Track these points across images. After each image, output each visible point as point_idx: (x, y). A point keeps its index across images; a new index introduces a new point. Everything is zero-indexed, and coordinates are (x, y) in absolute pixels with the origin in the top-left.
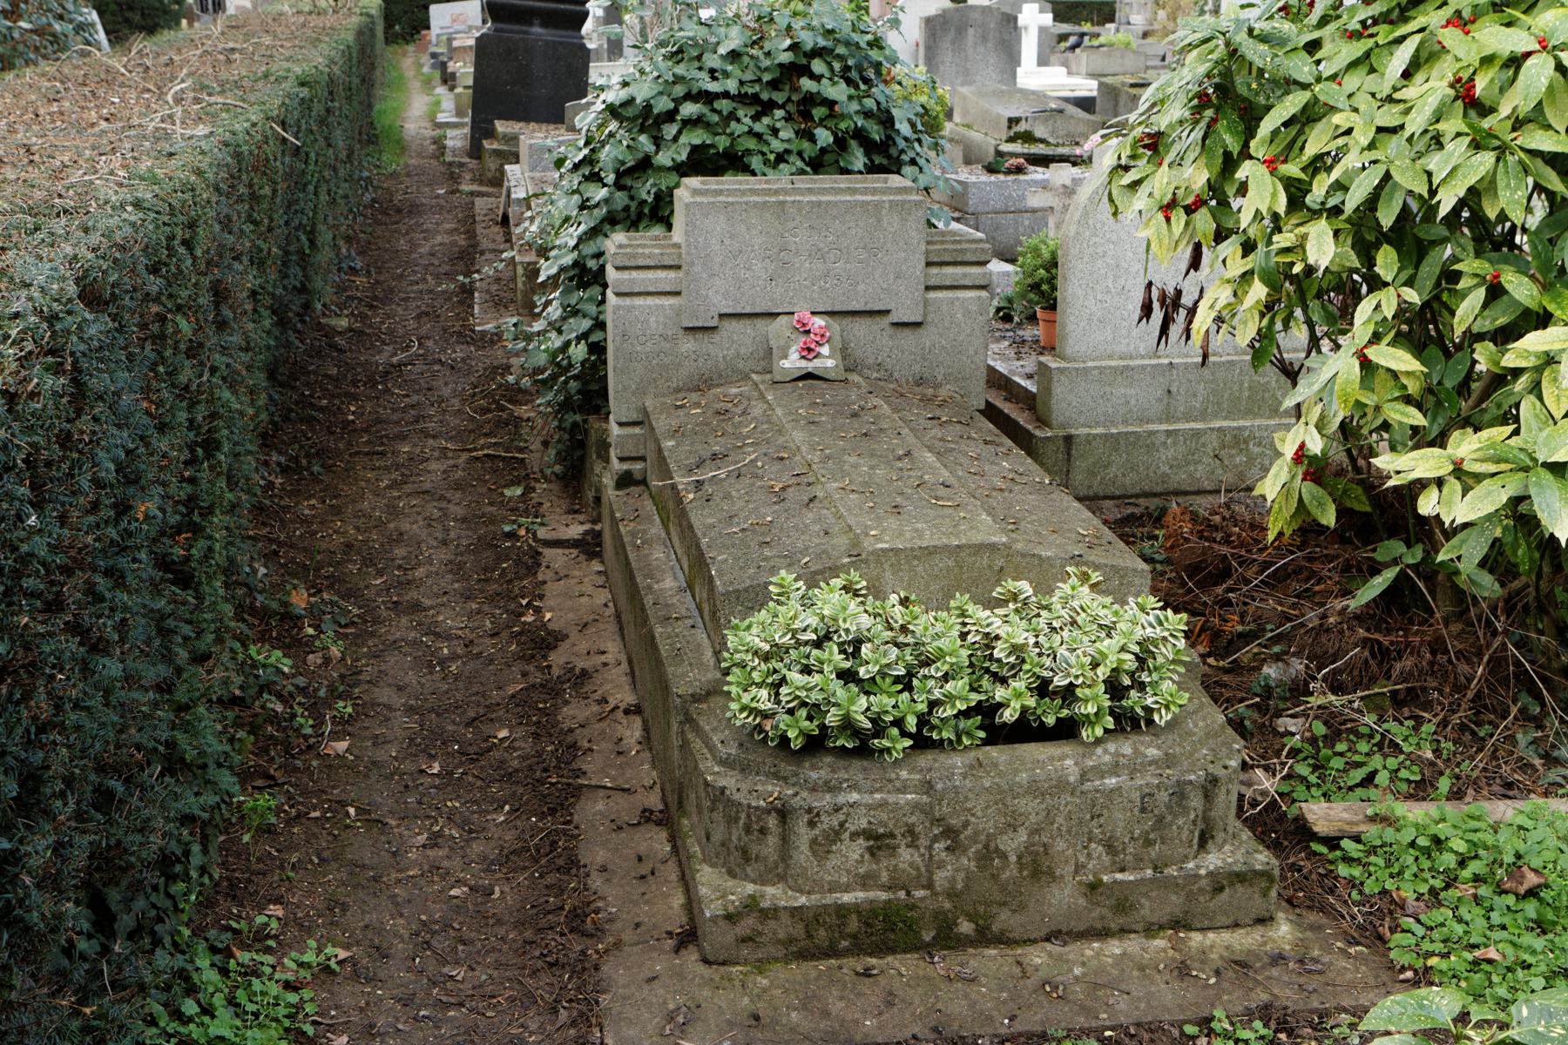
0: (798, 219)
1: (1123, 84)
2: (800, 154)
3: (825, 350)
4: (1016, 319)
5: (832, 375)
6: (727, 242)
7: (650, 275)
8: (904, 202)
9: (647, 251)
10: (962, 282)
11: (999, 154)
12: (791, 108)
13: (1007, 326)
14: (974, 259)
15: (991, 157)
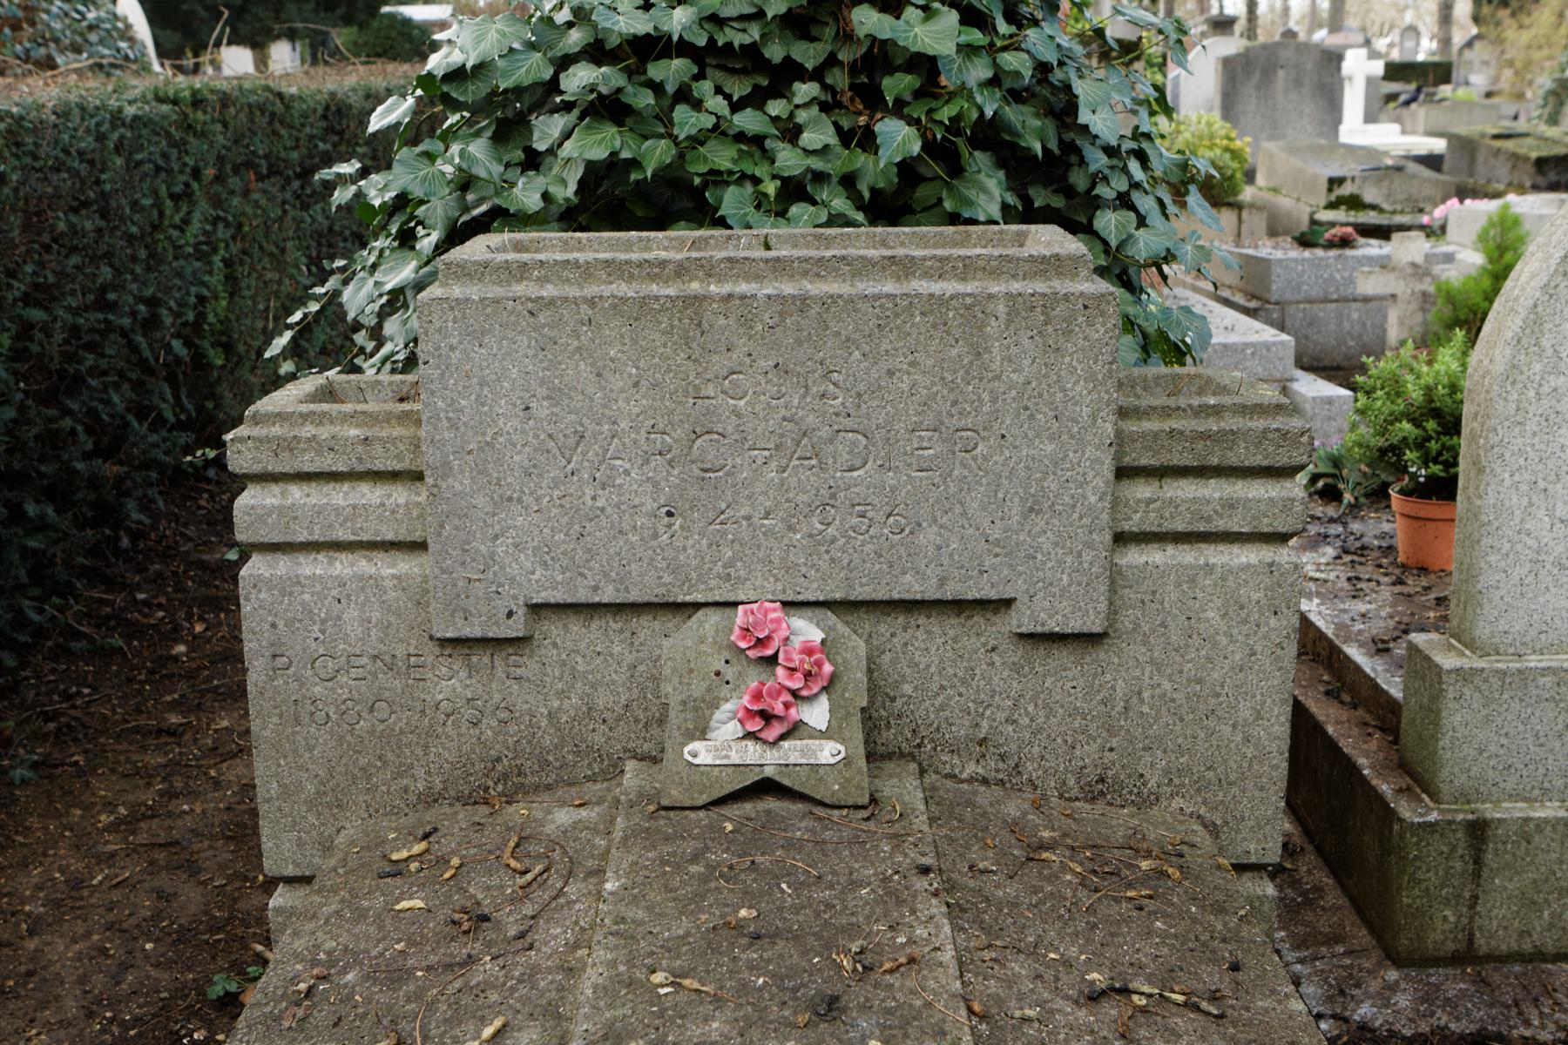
0: (743, 346)
1: (1483, 135)
2: (849, 182)
3: (817, 714)
4: (1348, 497)
5: (833, 789)
6: (541, 409)
7: (339, 496)
8: (1051, 300)
9: (324, 433)
10: (1221, 525)
11: (1313, 222)
12: (839, 79)
13: (1331, 511)
14: (1258, 460)
15: (1304, 226)
